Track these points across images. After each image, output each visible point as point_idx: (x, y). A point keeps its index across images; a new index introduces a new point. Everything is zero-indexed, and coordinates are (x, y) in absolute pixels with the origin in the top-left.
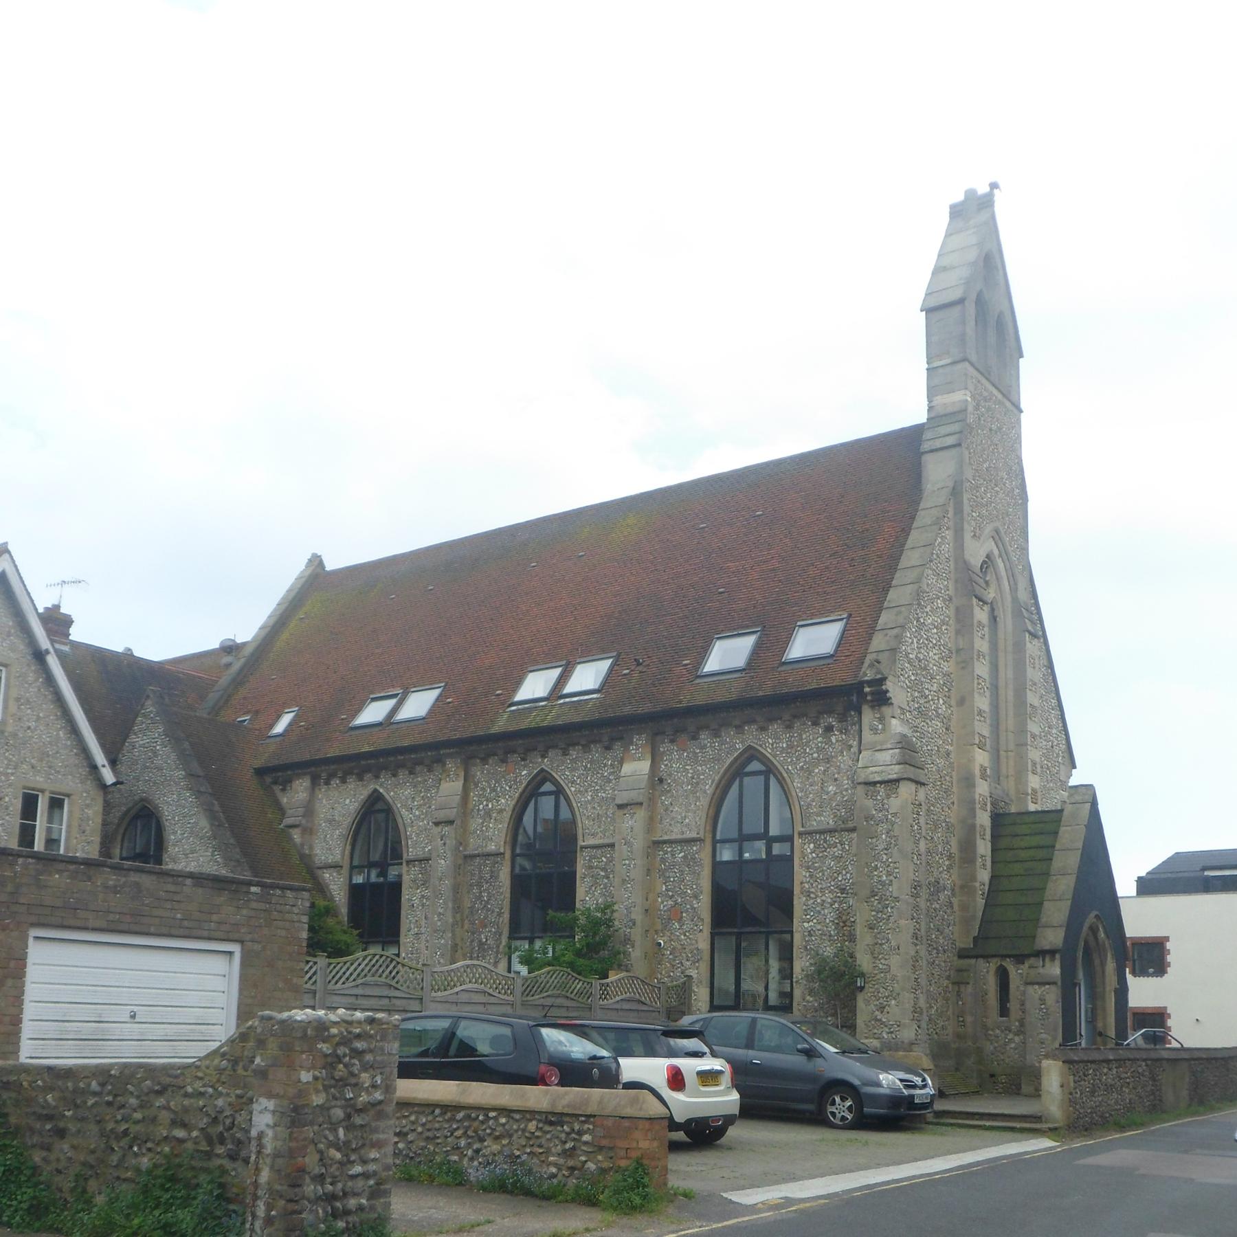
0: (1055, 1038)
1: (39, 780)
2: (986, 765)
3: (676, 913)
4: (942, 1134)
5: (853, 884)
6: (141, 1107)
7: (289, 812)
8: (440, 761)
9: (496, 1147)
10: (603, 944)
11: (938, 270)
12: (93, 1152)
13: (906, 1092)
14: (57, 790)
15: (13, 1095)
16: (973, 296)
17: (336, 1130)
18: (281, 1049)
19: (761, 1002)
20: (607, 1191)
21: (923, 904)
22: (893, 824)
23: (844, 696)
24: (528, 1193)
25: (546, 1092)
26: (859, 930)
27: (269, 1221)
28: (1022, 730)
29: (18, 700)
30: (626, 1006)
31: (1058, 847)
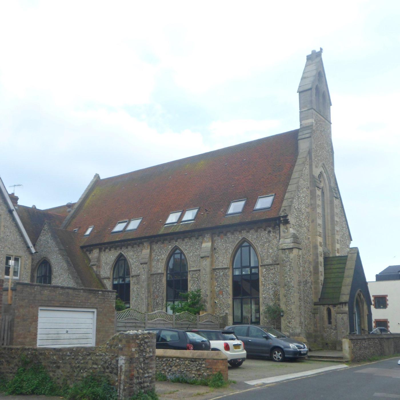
0: (347, 331)
1: (11, 252)
2: (322, 241)
3: (221, 292)
4: (310, 363)
5: (278, 282)
6: (83, 359)
7: (92, 261)
8: (142, 243)
9: (176, 369)
10: (198, 302)
11: (303, 78)
12: (69, 372)
13: (298, 350)
14: (17, 255)
15: (43, 357)
16: (315, 86)
17: (141, 364)
18: (126, 342)
19: (250, 320)
20: (210, 381)
21: (302, 288)
22: (291, 262)
23: (275, 221)
24: (186, 382)
25: (191, 352)
26: (281, 297)
27: (124, 390)
28: (333, 229)
29: (4, 226)
30: (207, 323)
31: (346, 268)
